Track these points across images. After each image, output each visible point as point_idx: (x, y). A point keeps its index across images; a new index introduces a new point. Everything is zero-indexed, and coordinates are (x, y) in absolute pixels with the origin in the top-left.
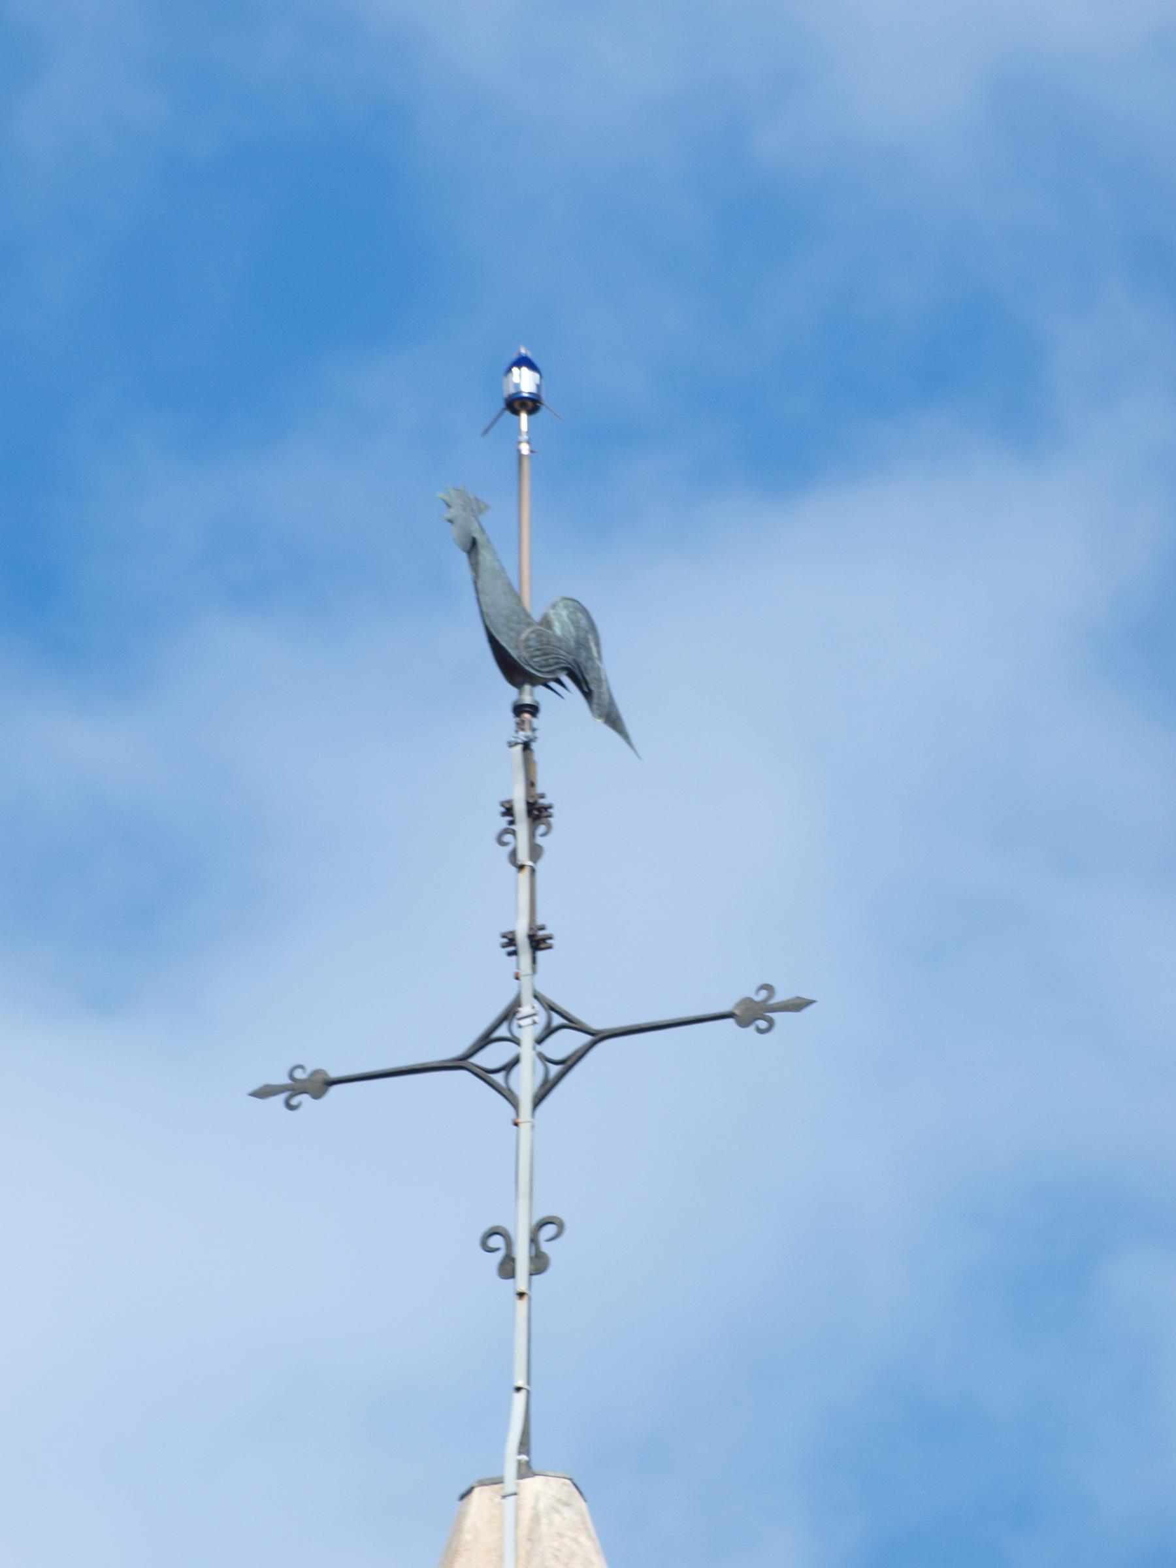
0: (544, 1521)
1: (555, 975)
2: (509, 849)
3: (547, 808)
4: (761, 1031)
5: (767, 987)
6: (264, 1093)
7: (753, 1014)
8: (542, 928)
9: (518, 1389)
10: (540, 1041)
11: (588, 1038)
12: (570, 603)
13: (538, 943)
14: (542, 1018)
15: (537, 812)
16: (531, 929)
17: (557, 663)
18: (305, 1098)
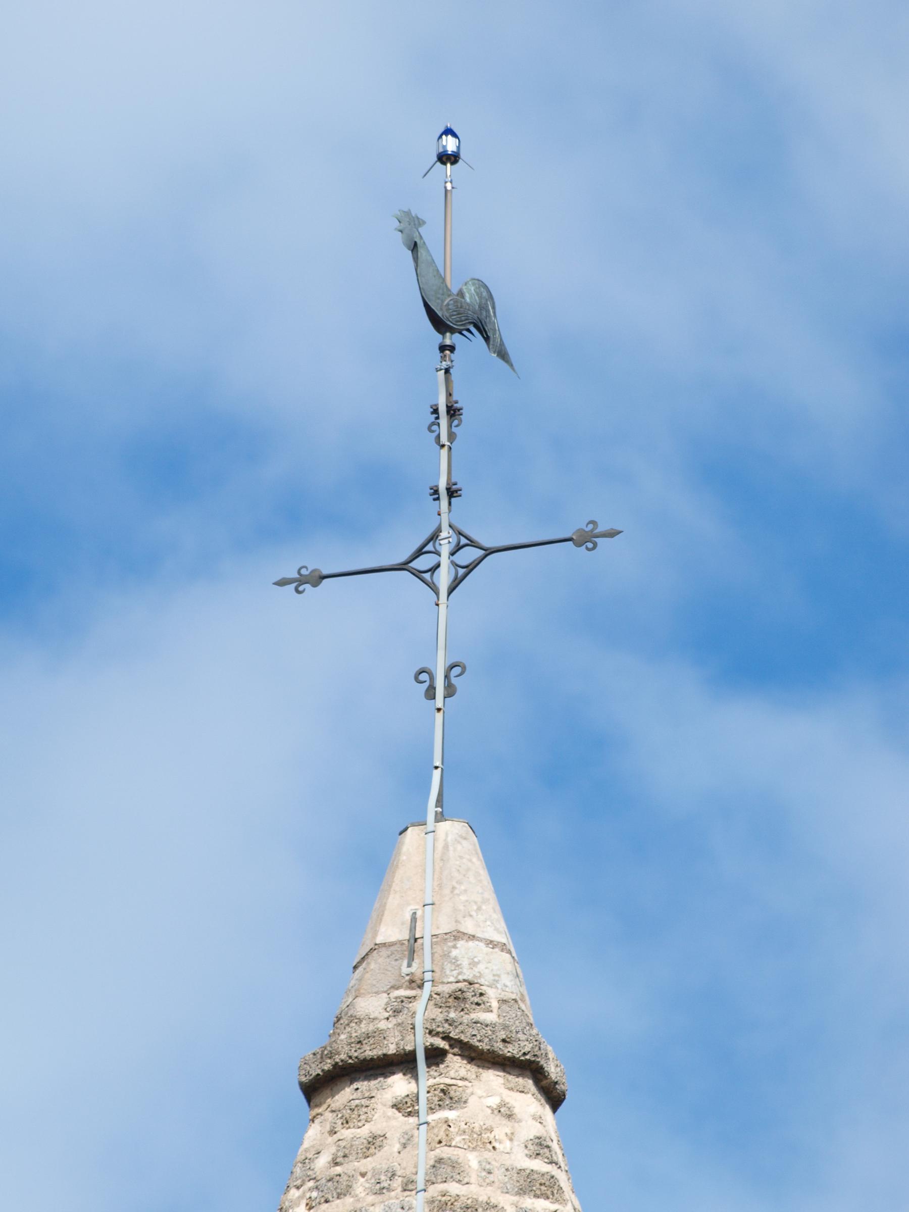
0: (451, 848)
2: (435, 434)
9: (436, 768)
11: (481, 553)
14: (454, 540)
16: (448, 484)
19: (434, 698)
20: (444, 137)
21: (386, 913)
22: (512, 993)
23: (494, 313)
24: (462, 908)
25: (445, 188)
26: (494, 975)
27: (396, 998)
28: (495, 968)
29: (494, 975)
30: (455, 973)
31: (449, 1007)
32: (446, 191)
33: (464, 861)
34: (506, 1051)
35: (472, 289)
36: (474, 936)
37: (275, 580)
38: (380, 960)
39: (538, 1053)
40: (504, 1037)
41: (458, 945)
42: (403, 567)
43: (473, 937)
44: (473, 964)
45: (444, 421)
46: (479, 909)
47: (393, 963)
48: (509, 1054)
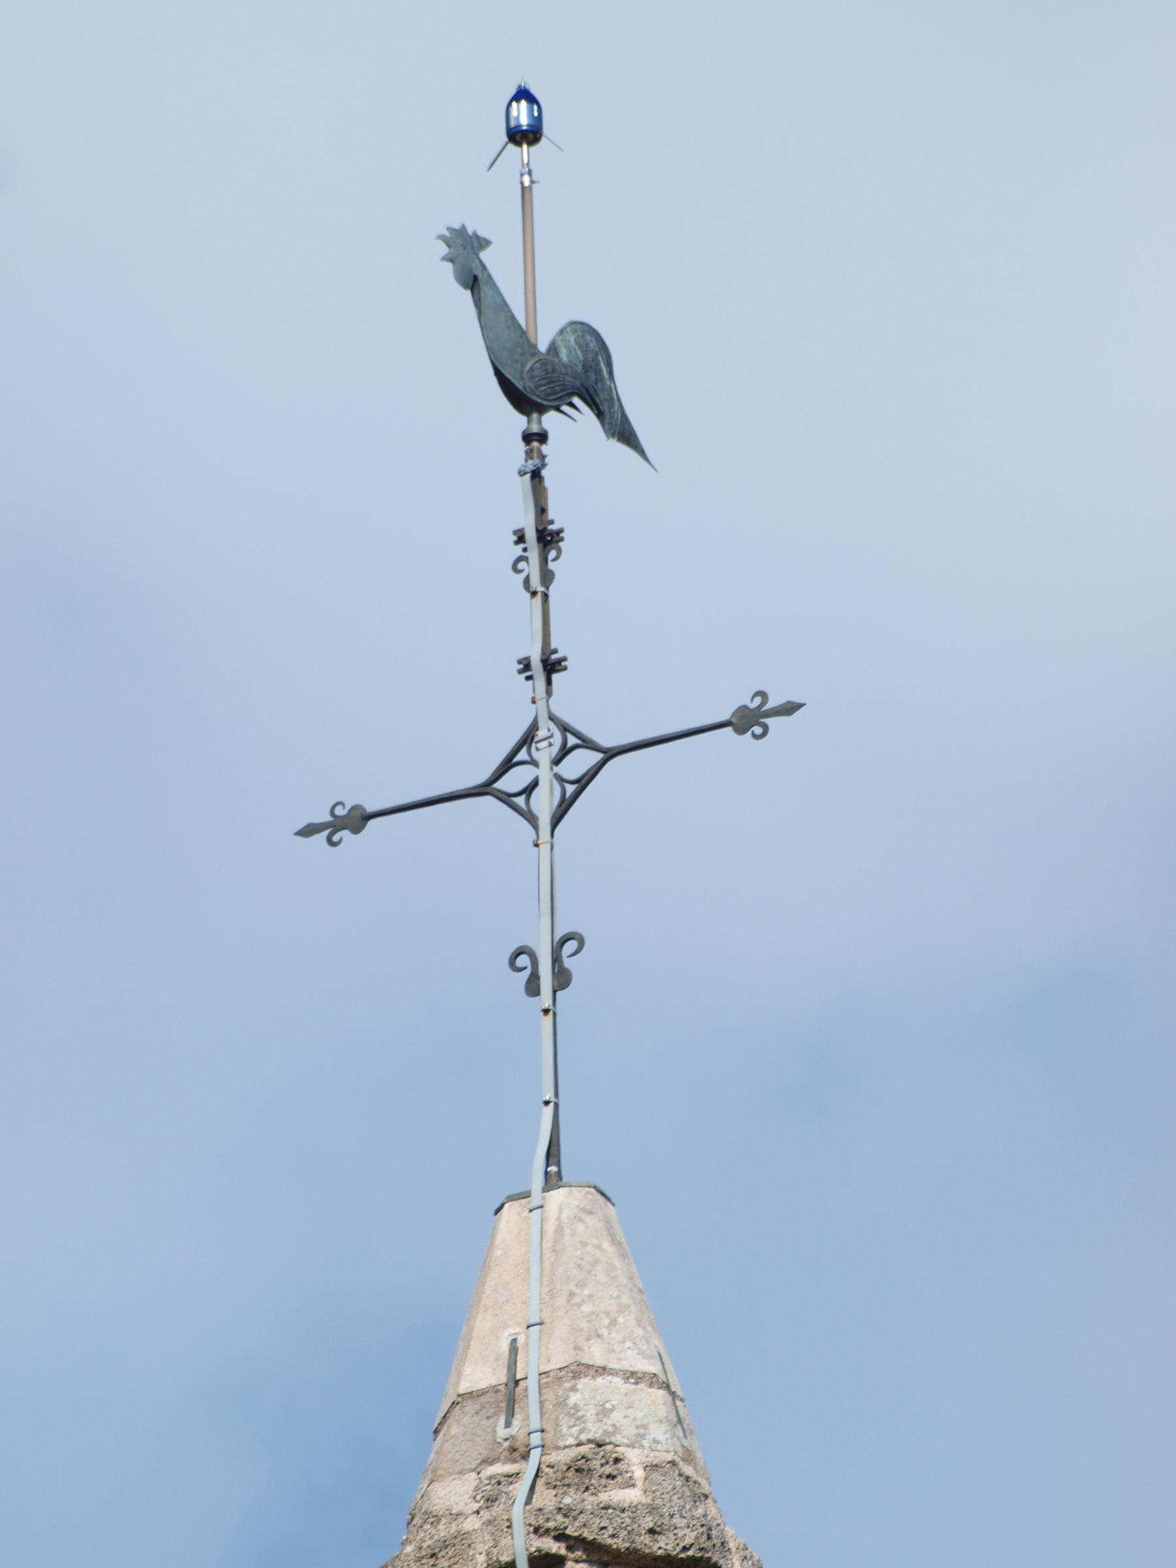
0: (567, 1231)
1: (571, 698)
2: (523, 576)
3: (559, 532)
4: (756, 737)
5: (762, 694)
6: (308, 831)
7: (747, 721)
8: (555, 651)
9: (547, 1103)
10: (557, 762)
11: (598, 757)
12: (579, 326)
13: (552, 666)
14: (557, 740)
15: (548, 539)
16: (543, 653)
17: (562, 390)
18: (345, 834)
19: (538, 994)
20: (514, 104)
21: (473, 1343)
22: (667, 1451)
23: (611, 373)
24: (585, 1325)
25: (522, 183)
26: (637, 1427)
27: (490, 1478)
28: (639, 1415)
29: (637, 1427)
30: (575, 1430)
31: (569, 1485)
32: (523, 188)
33: (589, 1248)
34: (655, 1548)
35: (572, 339)
36: (604, 1368)
37: (296, 830)
38: (466, 1420)
39: (708, 1544)
40: (651, 1525)
41: (579, 1386)
42: (483, 789)
43: (603, 1370)
44: (604, 1412)
45: (534, 555)
46: (613, 1323)
47: (484, 1422)
48: (660, 1552)
